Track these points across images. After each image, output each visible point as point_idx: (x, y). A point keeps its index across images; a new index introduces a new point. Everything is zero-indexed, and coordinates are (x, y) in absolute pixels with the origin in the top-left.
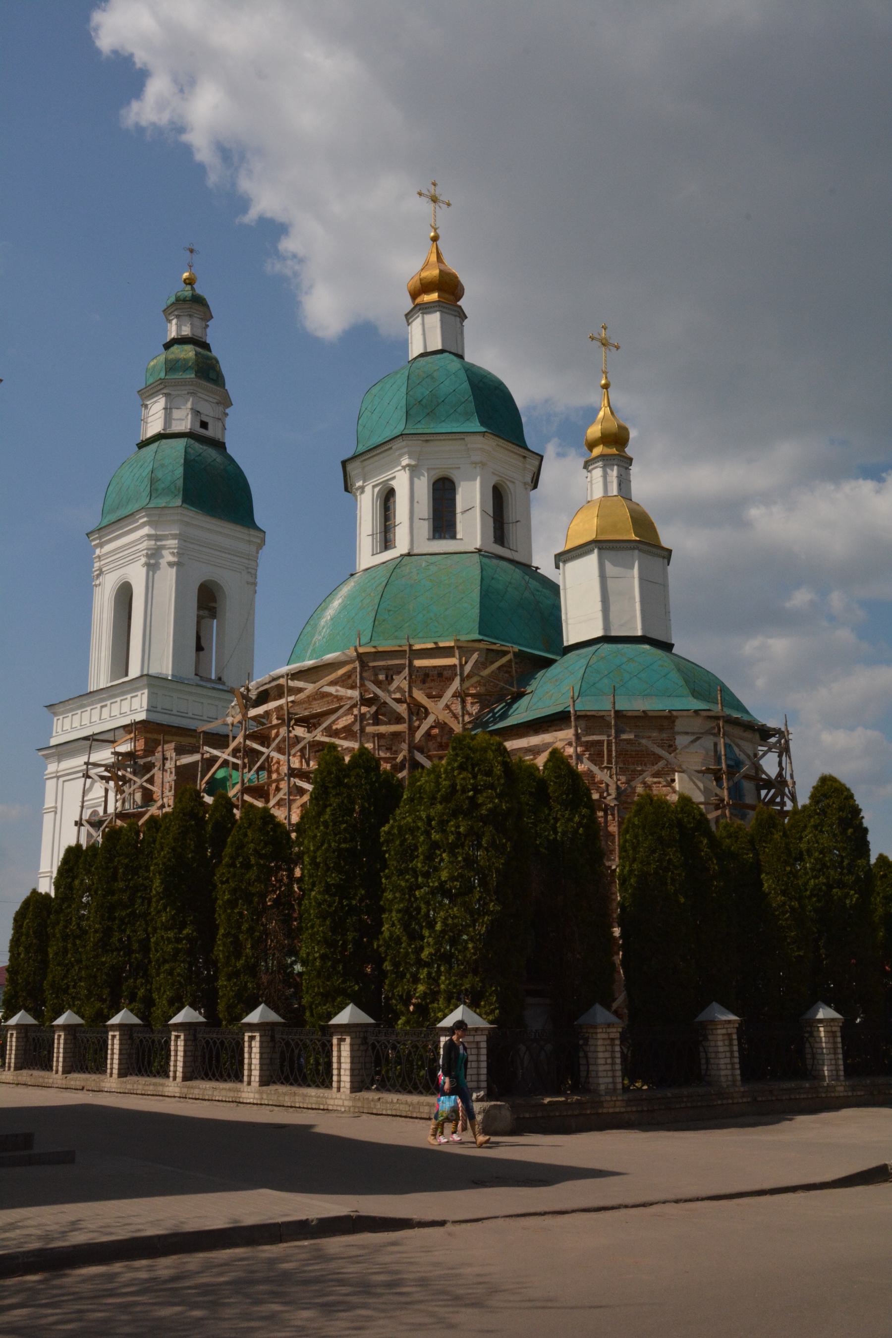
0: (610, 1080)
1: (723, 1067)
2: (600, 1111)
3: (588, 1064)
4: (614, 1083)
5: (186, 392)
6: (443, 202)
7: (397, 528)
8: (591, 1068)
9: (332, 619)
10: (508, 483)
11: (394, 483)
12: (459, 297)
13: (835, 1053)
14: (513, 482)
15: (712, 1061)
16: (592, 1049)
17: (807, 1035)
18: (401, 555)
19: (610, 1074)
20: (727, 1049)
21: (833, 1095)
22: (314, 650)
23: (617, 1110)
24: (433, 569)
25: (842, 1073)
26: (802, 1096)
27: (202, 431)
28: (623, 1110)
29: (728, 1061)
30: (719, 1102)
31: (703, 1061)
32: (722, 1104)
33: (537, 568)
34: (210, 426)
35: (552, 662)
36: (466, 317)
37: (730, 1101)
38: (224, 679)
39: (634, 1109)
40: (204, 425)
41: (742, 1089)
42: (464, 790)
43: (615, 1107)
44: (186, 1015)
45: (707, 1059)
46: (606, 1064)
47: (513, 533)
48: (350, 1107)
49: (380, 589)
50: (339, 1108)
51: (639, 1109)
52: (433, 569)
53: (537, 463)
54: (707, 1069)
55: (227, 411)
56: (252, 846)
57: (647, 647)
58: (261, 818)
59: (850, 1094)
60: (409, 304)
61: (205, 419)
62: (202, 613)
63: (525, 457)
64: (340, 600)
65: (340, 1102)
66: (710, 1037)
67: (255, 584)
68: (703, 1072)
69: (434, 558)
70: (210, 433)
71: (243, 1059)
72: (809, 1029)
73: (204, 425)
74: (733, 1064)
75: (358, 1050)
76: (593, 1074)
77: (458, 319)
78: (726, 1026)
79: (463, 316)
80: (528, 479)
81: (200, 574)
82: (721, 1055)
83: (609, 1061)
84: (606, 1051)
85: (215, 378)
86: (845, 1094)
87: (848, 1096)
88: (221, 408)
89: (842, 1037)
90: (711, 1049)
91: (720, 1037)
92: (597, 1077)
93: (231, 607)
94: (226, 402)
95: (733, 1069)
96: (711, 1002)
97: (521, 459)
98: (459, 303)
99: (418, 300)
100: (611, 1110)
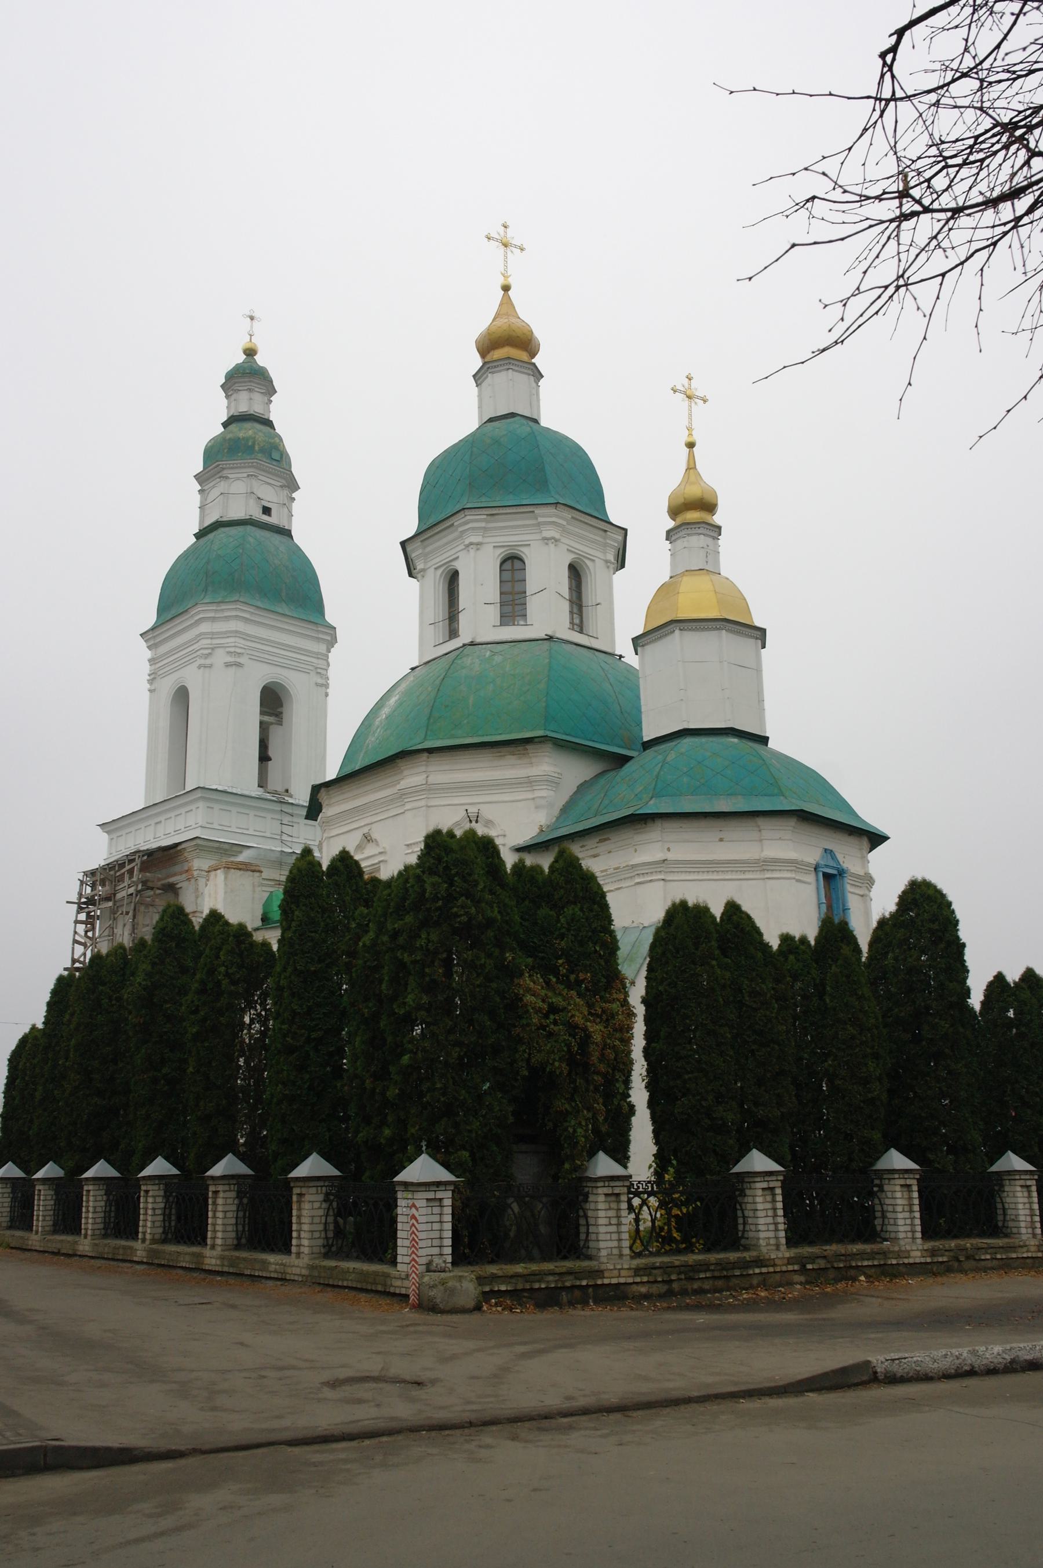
0: (615, 1244)
1: (761, 1227)
2: (599, 1282)
3: (588, 1225)
4: (620, 1248)
5: (245, 475)
6: (516, 246)
7: (460, 615)
8: (592, 1229)
9: (387, 718)
10: (587, 561)
11: (458, 565)
12: (533, 355)
13: (911, 1211)
14: (593, 561)
15: (750, 1221)
16: (592, 1206)
17: (875, 1189)
18: (464, 645)
19: (615, 1236)
20: (769, 1206)
21: (906, 1261)
22: (366, 752)
23: (622, 1280)
24: (498, 659)
25: (919, 1235)
26: (866, 1263)
27: (265, 518)
28: (630, 1280)
29: (770, 1220)
30: (757, 1271)
31: (1000, 1212)
32: (761, 1273)
33: (621, 657)
34: (273, 512)
35: (626, 759)
36: (542, 376)
37: (771, 1269)
38: (292, 791)
39: (645, 1279)
40: (267, 511)
41: (787, 1255)
42: (436, 899)
43: (619, 1276)
44: (159, 1166)
45: (1004, 1209)
46: (610, 1224)
47: (594, 618)
48: (307, 1276)
49: (438, 682)
50: (296, 1278)
51: (651, 1279)
52: (498, 659)
53: (620, 538)
54: (744, 1231)
55: (294, 495)
56: (222, 969)
57: (736, 740)
58: (234, 936)
59: (929, 1260)
60: (477, 362)
61: (267, 505)
62: (266, 718)
63: (606, 531)
64: (397, 698)
65: (297, 1271)
66: (748, 1192)
67: (327, 686)
68: (582, 1243)
69: (499, 647)
70: (273, 520)
71: (920, 1197)
72: (877, 1182)
73: (267, 511)
74: (776, 1224)
75: (320, 1208)
76: (593, 1237)
77: (532, 378)
78: (766, 1179)
79: (538, 375)
80: (611, 557)
81: (258, 676)
82: (760, 1214)
83: (770, 1213)
84: (610, 1209)
85: (278, 458)
86: (923, 1260)
87: (927, 1263)
88: (286, 492)
89: (919, 1191)
90: (749, 1206)
91: (760, 1192)
92: (895, 1224)
93: (298, 712)
94: (292, 485)
95: (776, 1230)
96: (750, 1150)
97: (602, 533)
98: (533, 361)
99: (488, 358)
100: (614, 1281)
